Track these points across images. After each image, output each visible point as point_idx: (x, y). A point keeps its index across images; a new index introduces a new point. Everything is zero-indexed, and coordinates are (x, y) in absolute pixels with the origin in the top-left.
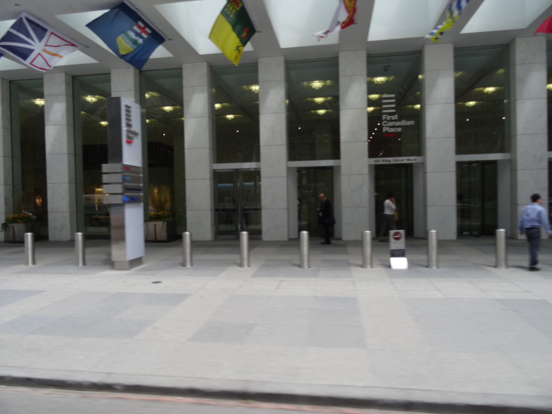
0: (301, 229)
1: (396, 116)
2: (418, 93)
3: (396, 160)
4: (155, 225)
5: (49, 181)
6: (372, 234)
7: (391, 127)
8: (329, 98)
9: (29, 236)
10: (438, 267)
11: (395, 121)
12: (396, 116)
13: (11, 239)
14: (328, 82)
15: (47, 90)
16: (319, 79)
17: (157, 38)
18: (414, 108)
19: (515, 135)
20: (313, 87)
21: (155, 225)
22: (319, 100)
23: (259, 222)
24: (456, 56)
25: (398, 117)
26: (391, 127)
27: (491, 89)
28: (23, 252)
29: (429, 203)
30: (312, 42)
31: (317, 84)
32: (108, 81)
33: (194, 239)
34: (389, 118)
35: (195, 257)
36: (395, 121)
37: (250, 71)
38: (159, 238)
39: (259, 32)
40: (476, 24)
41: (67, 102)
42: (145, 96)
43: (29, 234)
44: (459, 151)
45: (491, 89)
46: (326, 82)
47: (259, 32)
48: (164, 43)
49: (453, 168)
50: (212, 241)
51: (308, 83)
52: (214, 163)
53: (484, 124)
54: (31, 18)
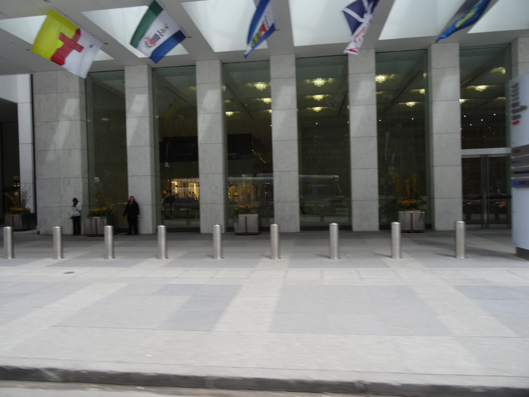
0: (158, 224)
2: (228, 101)
4: (411, 215)
5: (130, 173)
6: (221, 227)
9: (109, 228)
10: (339, 258)
13: (244, 231)
14: (330, 80)
15: (274, 72)
16: (322, 77)
17: (179, 37)
19: (432, 134)
20: (315, 84)
21: (411, 215)
22: (319, 97)
23: (350, 215)
24: (298, 66)
27: (482, 87)
28: (270, 245)
31: (319, 82)
33: (286, 229)
35: (117, 249)
37: (261, 68)
38: (415, 228)
39: (279, 30)
42: (506, 71)
43: (109, 227)
44: (465, 145)
45: (482, 87)
46: (328, 79)
47: (279, 30)
48: (184, 41)
50: (71, 235)
53: (484, 121)
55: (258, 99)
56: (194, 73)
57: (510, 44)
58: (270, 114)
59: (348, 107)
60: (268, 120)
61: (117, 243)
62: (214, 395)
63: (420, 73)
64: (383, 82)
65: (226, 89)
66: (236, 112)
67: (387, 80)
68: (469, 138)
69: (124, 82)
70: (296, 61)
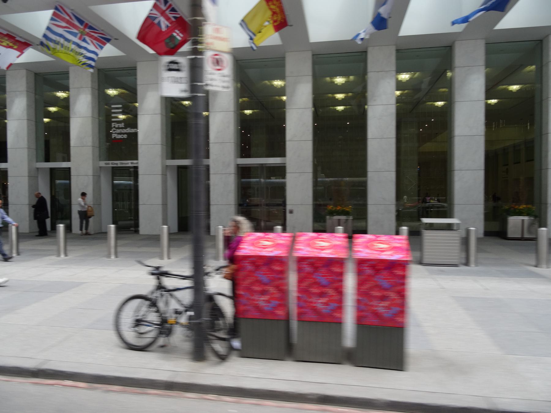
1: (123, 124)
3: (122, 164)
7: (118, 134)
8: (350, 94)
11: (122, 128)
12: (123, 124)
14: (352, 78)
15: (73, 82)
18: (434, 105)
20: (336, 83)
22: (340, 96)
24: (314, 63)
25: (124, 125)
26: (118, 134)
27: (514, 88)
28: (57, 244)
29: (212, 202)
30: (345, 35)
31: (340, 80)
32: (68, 78)
34: (117, 126)
36: (122, 128)
39: (291, 26)
40: (513, 20)
41: (93, 95)
45: (514, 88)
46: (349, 77)
47: (291, 26)
49: (232, 169)
51: (331, 79)
52: (238, 158)
54: (62, 6)
55: (277, 97)
56: (365, 61)
57: (36, 74)
58: (6, 123)
59: (366, 107)
60: (283, 120)
61: (120, 242)
62: (53, 385)
63: (445, 72)
64: (407, 81)
65: (241, 85)
66: (255, 111)
67: (411, 79)
68: (245, 148)
69: (136, 79)
70: (313, 58)
